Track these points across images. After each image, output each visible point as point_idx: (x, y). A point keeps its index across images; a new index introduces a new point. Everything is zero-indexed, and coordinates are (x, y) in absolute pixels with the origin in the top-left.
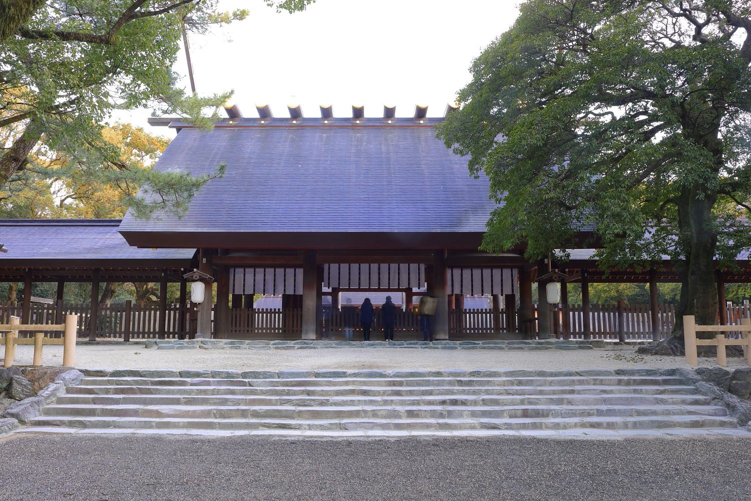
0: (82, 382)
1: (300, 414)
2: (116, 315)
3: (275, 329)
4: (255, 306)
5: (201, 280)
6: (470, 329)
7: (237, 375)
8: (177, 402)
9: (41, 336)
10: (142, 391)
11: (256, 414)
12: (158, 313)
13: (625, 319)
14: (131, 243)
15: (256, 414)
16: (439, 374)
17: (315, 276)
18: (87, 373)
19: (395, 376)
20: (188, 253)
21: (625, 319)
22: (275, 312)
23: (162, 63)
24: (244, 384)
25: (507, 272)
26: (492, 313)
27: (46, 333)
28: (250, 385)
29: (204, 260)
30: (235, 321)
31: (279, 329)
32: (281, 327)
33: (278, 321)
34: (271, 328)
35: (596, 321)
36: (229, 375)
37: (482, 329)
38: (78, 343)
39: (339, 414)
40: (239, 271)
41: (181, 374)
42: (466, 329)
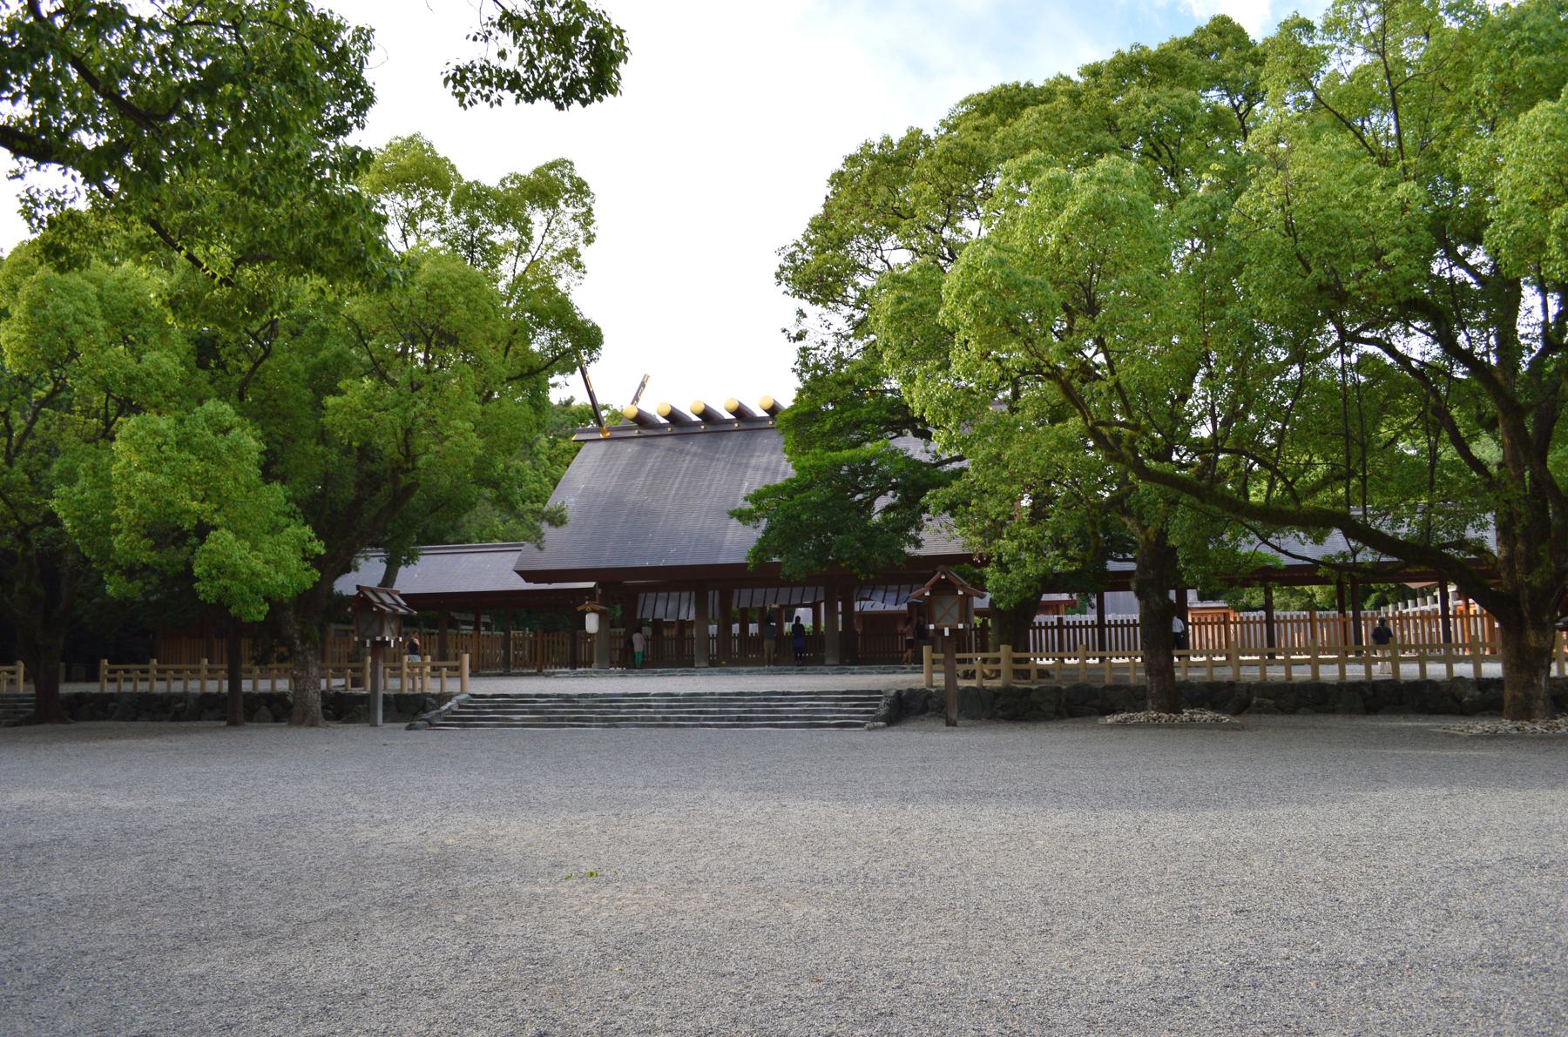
5: (594, 611)
18: (474, 696)
20: (591, 585)
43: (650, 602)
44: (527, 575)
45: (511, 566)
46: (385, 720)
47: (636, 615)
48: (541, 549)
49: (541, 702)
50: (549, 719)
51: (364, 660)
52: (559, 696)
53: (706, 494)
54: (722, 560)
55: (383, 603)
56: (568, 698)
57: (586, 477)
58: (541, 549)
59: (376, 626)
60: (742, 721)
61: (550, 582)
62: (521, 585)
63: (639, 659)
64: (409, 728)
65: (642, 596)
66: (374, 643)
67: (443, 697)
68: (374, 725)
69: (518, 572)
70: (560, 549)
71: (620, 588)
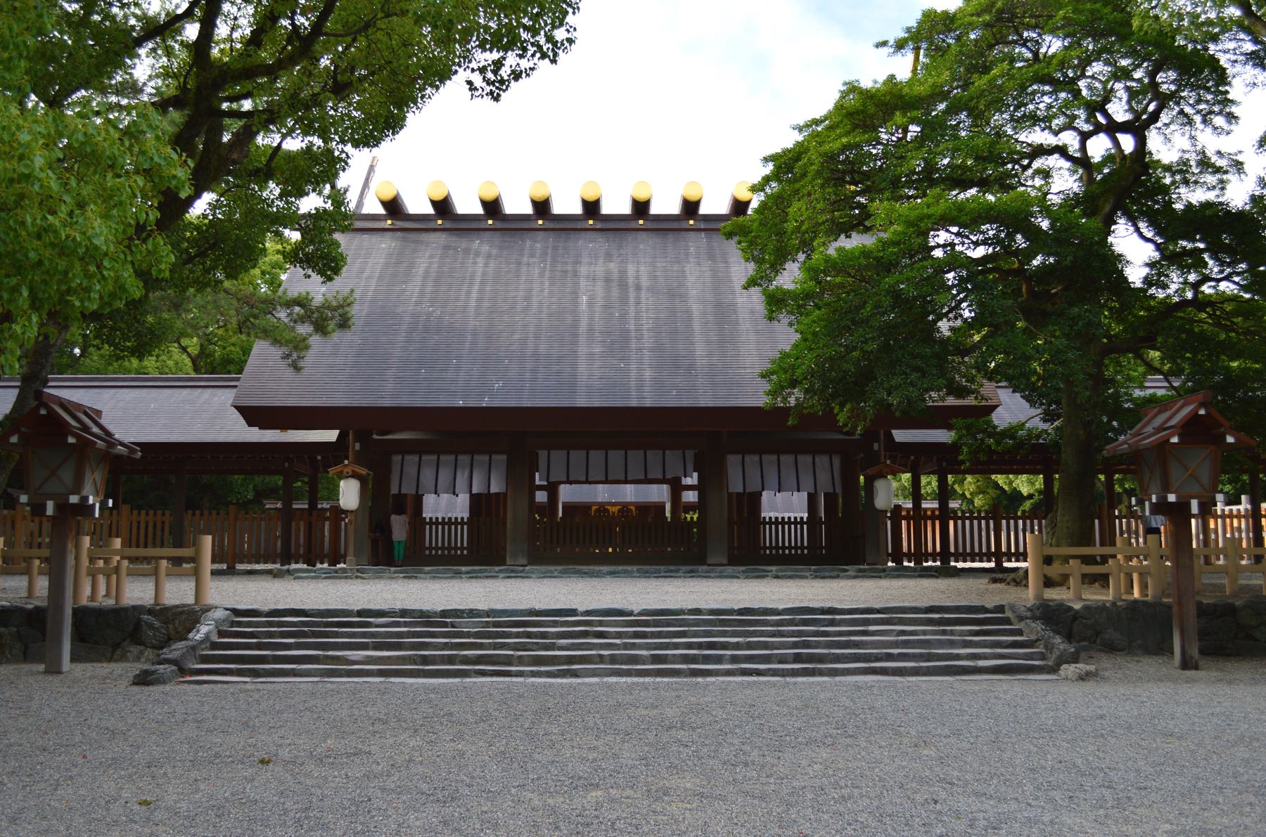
0: (233, 624)
1: (521, 661)
2: (1129, 524)
3: (456, 548)
4: (427, 514)
5: (354, 475)
6: (771, 548)
7: (435, 614)
8: (364, 647)
9: (164, 563)
10: (315, 634)
11: (466, 660)
12: (937, 523)
13: (929, 529)
14: (250, 423)
15: (466, 660)
16: (697, 611)
17: (520, 471)
18: (236, 612)
19: (640, 614)
20: (331, 436)
21: (929, 529)
22: (456, 523)
23: (1149, 309)
24: (445, 625)
25: (822, 461)
26: (937, 518)
27: (169, 559)
28: (453, 626)
29: (357, 446)
30: (392, 540)
31: (462, 548)
32: (938, 549)
33: (462, 537)
34: (450, 548)
35: (984, 534)
36: (422, 614)
37: (443, 548)
38: (214, 573)
39: (571, 660)
40: (397, 459)
41: (360, 613)
42: (765, 548)
43: (411, 471)
44: (253, 415)
45: (230, 402)
46: (74, 659)
47: (542, 475)
48: (297, 369)
49: (379, 627)
50: (425, 660)
51: (196, 544)
52: (404, 613)
53: (526, 309)
54: (581, 402)
55: (86, 429)
56: (424, 617)
57: (366, 263)
58: (297, 369)
59: (67, 475)
60: (810, 663)
61: (284, 427)
62: (239, 431)
63: (399, 552)
64: (144, 679)
65: (397, 459)
66: (63, 507)
67: (188, 617)
68: (54, 669)
69: (236, 407)
70: (329, 374)
71: (383, 438)
